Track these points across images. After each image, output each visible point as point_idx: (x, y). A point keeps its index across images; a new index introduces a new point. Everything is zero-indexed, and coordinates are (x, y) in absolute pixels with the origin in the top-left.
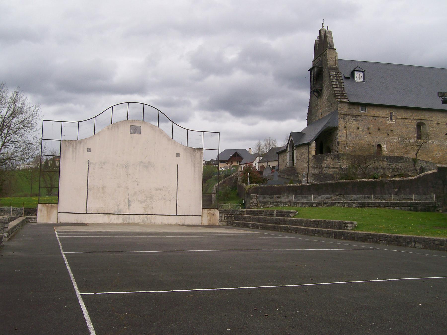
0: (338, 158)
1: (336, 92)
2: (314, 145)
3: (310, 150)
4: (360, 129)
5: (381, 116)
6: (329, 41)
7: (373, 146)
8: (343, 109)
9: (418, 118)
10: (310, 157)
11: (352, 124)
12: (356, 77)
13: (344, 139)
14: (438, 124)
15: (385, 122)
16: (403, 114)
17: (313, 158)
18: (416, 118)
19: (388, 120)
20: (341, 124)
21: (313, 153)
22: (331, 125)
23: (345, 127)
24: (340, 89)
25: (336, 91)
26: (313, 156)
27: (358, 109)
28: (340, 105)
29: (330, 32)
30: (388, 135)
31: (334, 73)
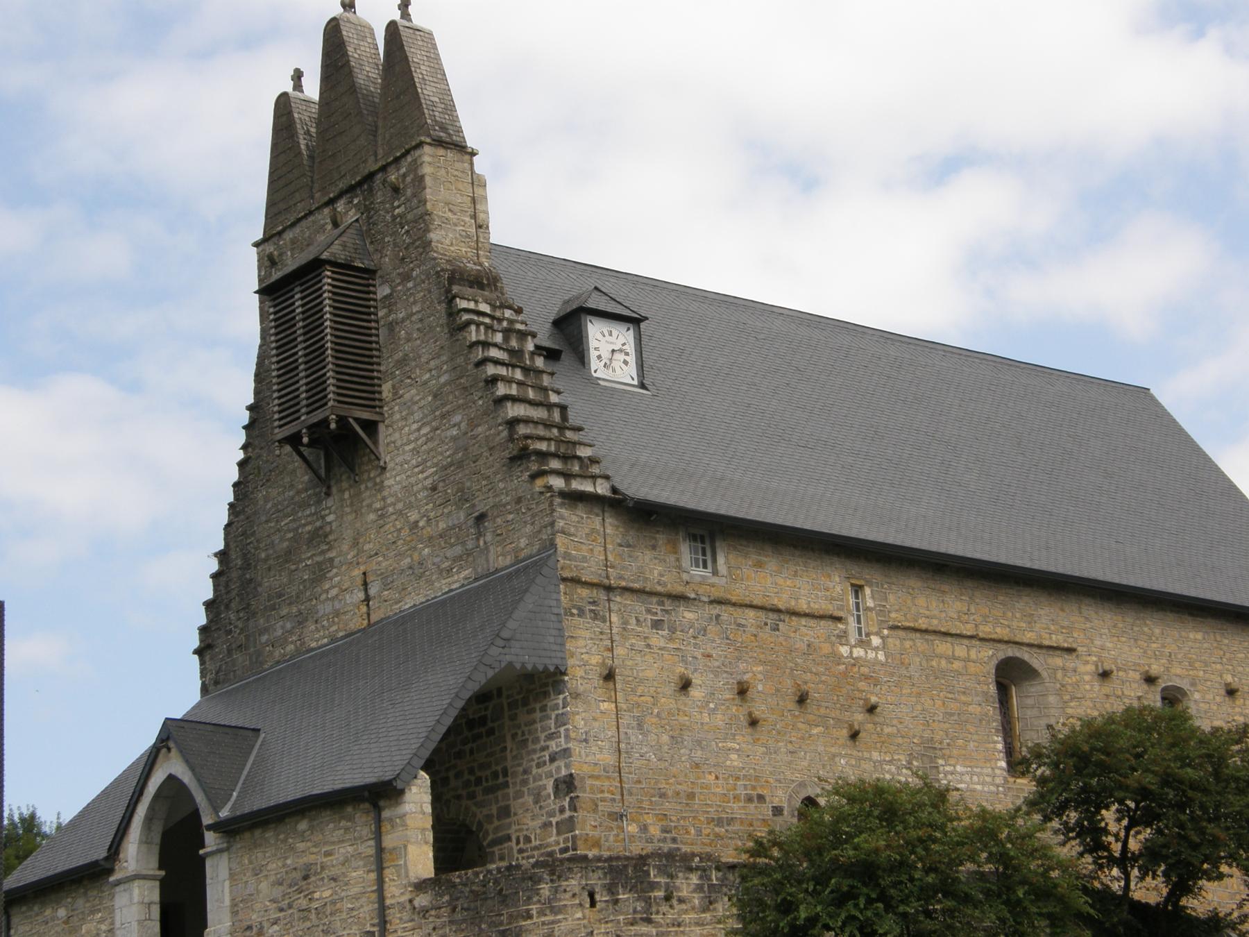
0: (642, 886)
1: (522, 430)
2: (418, 799)
3: (389, 841)
4: (696, 693)
5: (803, 606)
6: (427, 92)
7: (778, 811)
8: (588, 543)
9: (1001, 632)
10: (396, 892)
11: (649, 658)
12: (593, 354)
13: (608, 758)
14: (1105, 675)
15: (826, 648)
16: (921, 601)
17: (422, 900)
18: (986, 630)
19: (843, 637)
20: (583, 652)
21: (420, 860)
22: (525, 657)
23: (609, 676)
24: (538, 413)
25: (527, 421)
26: (421, 886)
27: (675, 550)
28: (567, 516)
29: (428, 37)
30: (854, 736)
31: (484, 307)
